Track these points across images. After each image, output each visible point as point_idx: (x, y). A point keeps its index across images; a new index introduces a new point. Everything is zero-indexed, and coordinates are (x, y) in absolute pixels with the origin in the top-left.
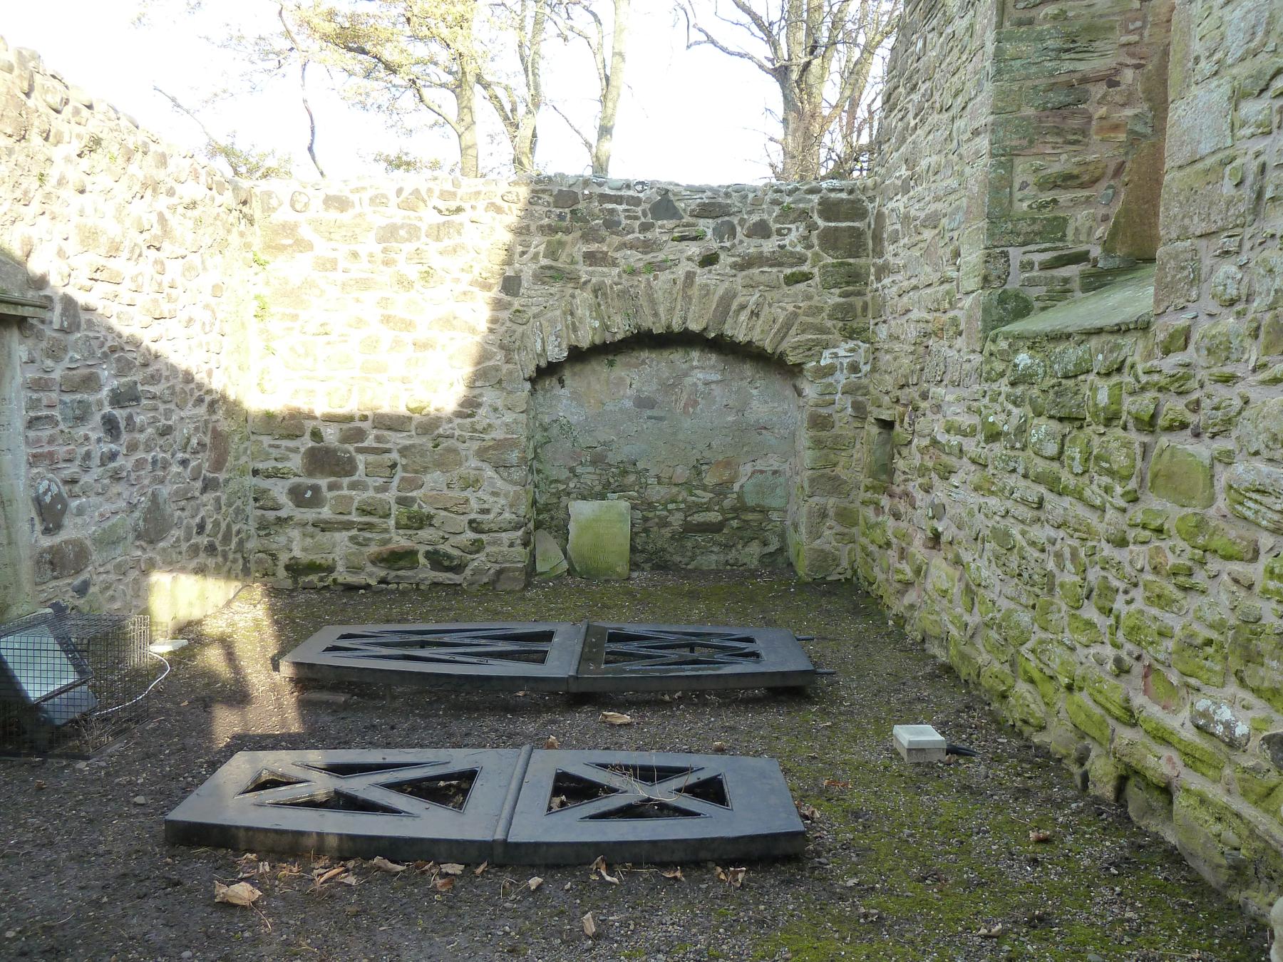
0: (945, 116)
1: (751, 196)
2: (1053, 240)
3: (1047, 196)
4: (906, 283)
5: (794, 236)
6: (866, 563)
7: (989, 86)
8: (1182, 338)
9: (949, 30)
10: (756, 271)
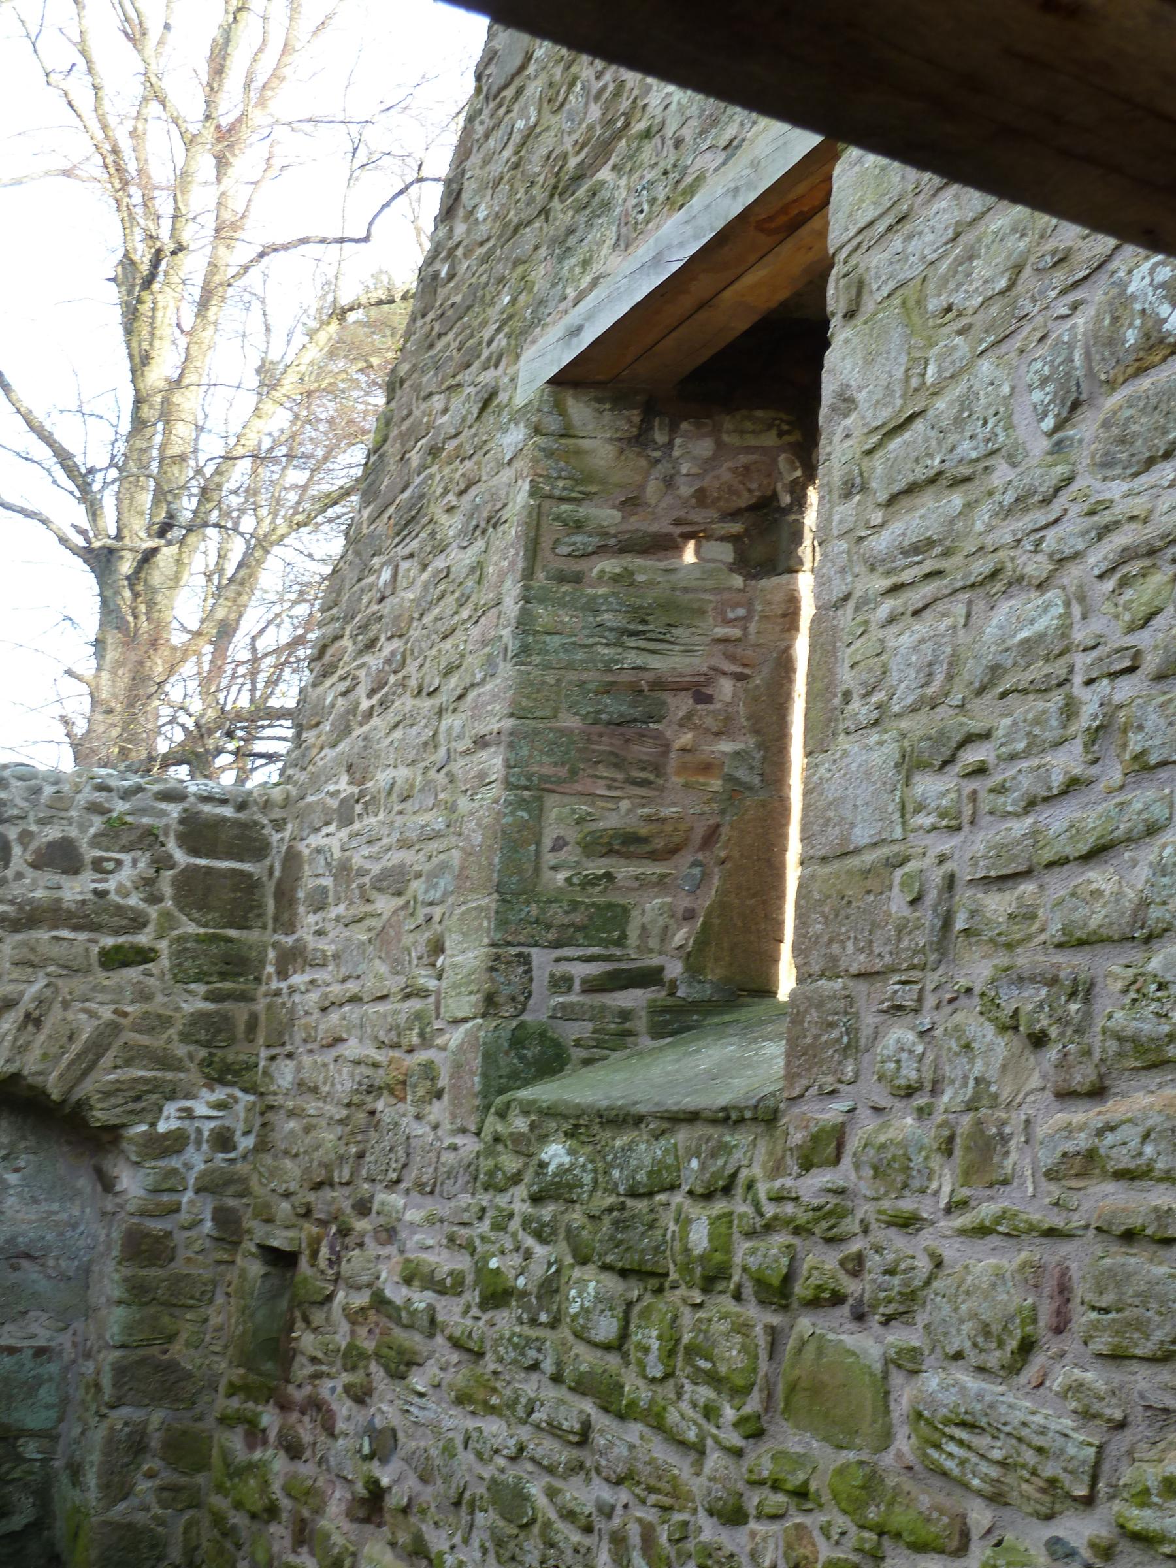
0: (426, 704)
1: (48, 790)
2: (605, 943)
3: (597, 867)
4: (336, 989)
5: (126, 875)
6: (221, 1552)
7: (506, 670)
8: (826, 1147)
9: (440, 563)
10: (44, 935)
